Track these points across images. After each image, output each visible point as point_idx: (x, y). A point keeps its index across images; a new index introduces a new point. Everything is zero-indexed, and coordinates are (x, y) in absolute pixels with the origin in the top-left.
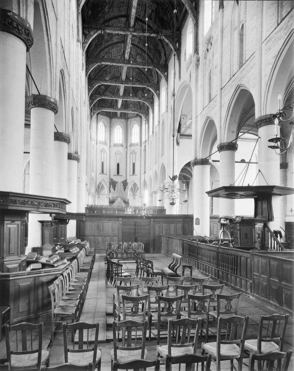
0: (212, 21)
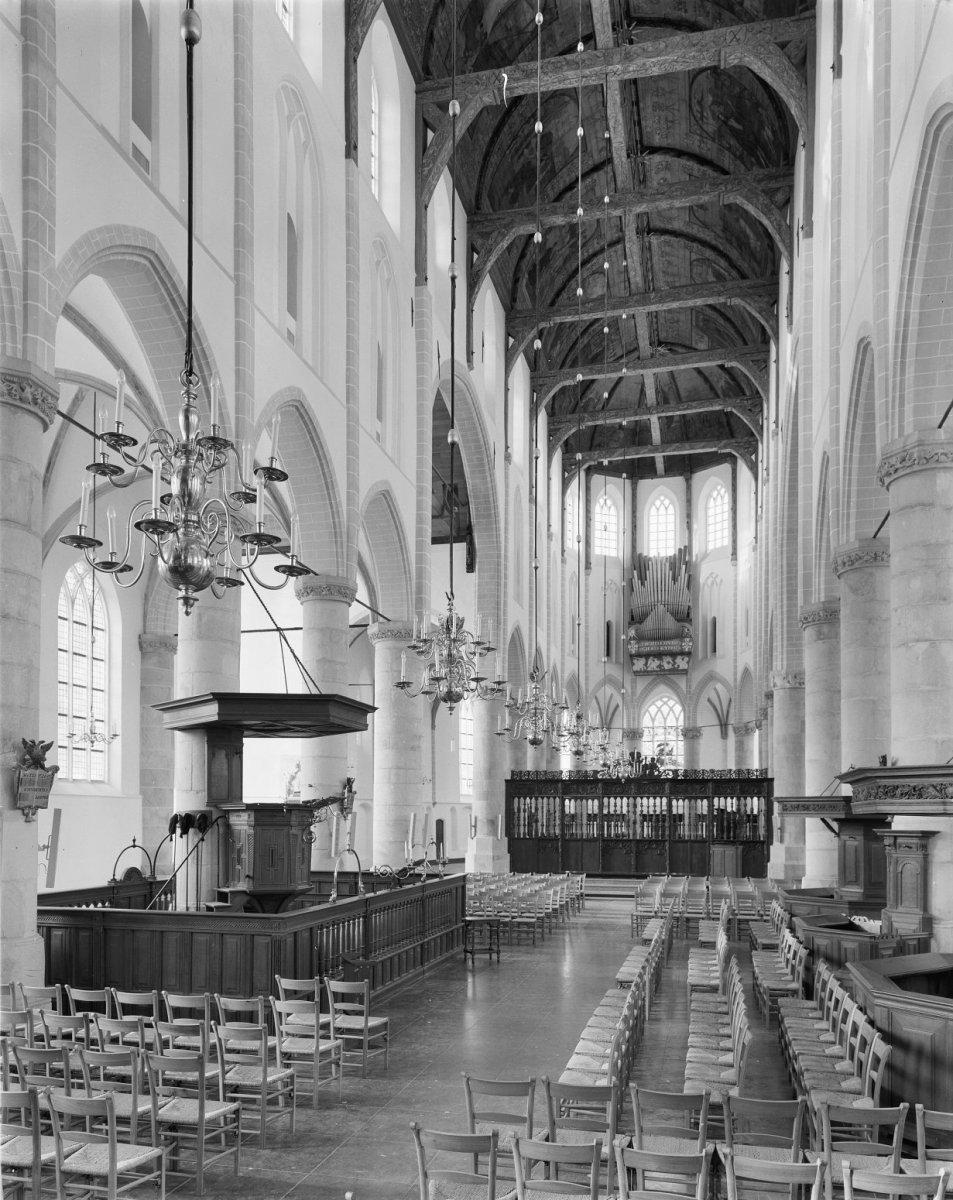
0: (306, 363)
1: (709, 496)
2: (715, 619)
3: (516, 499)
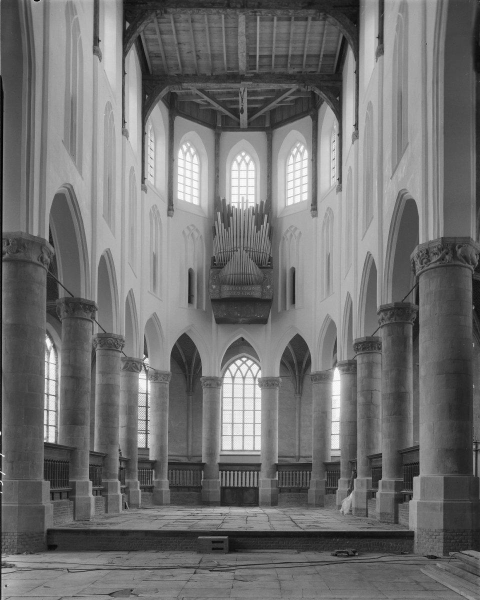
1: (289, 153)
3: (130, 176)
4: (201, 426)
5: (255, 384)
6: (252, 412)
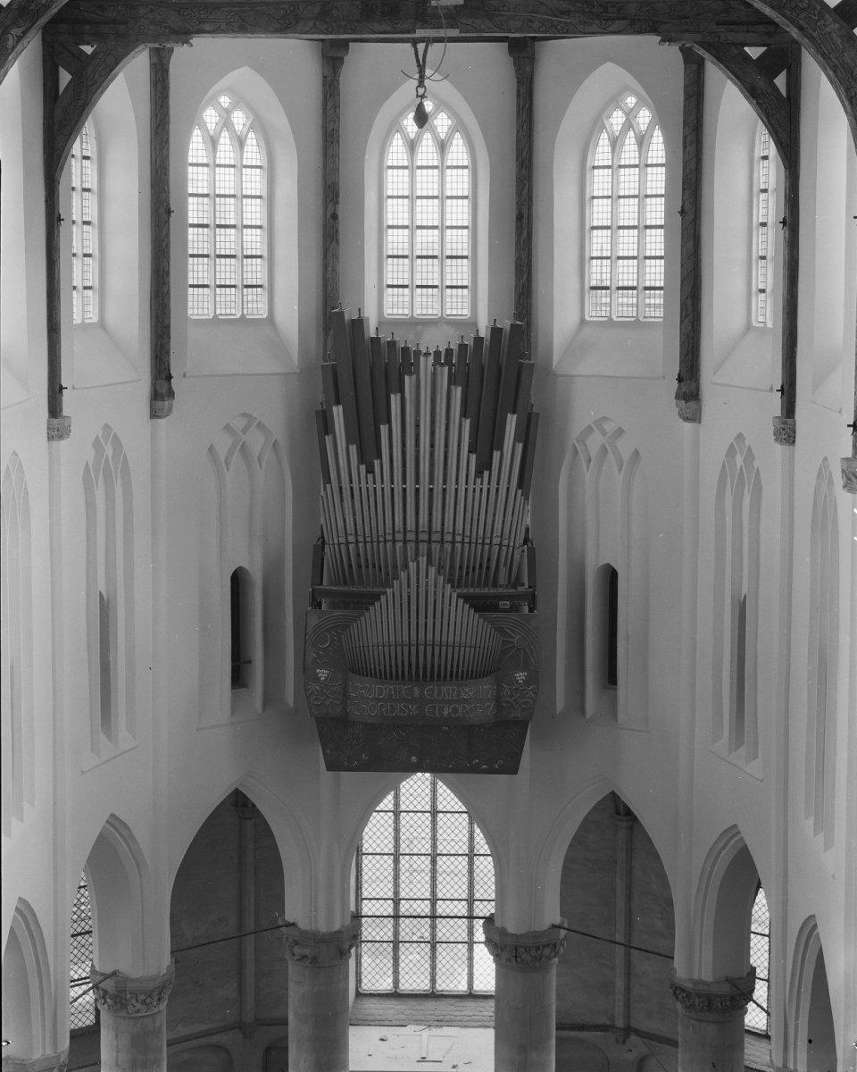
2: (611, 577)
4: (294, 546)
5: (470, 944)
6: (464, 861)
